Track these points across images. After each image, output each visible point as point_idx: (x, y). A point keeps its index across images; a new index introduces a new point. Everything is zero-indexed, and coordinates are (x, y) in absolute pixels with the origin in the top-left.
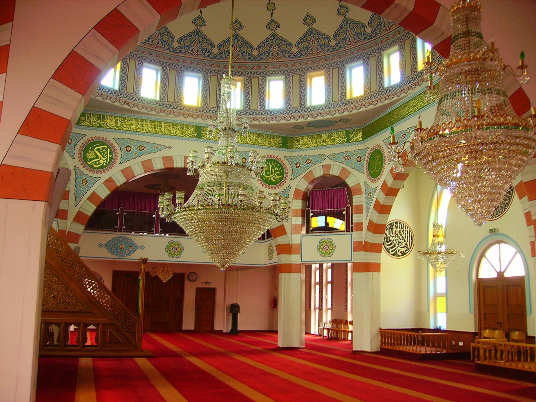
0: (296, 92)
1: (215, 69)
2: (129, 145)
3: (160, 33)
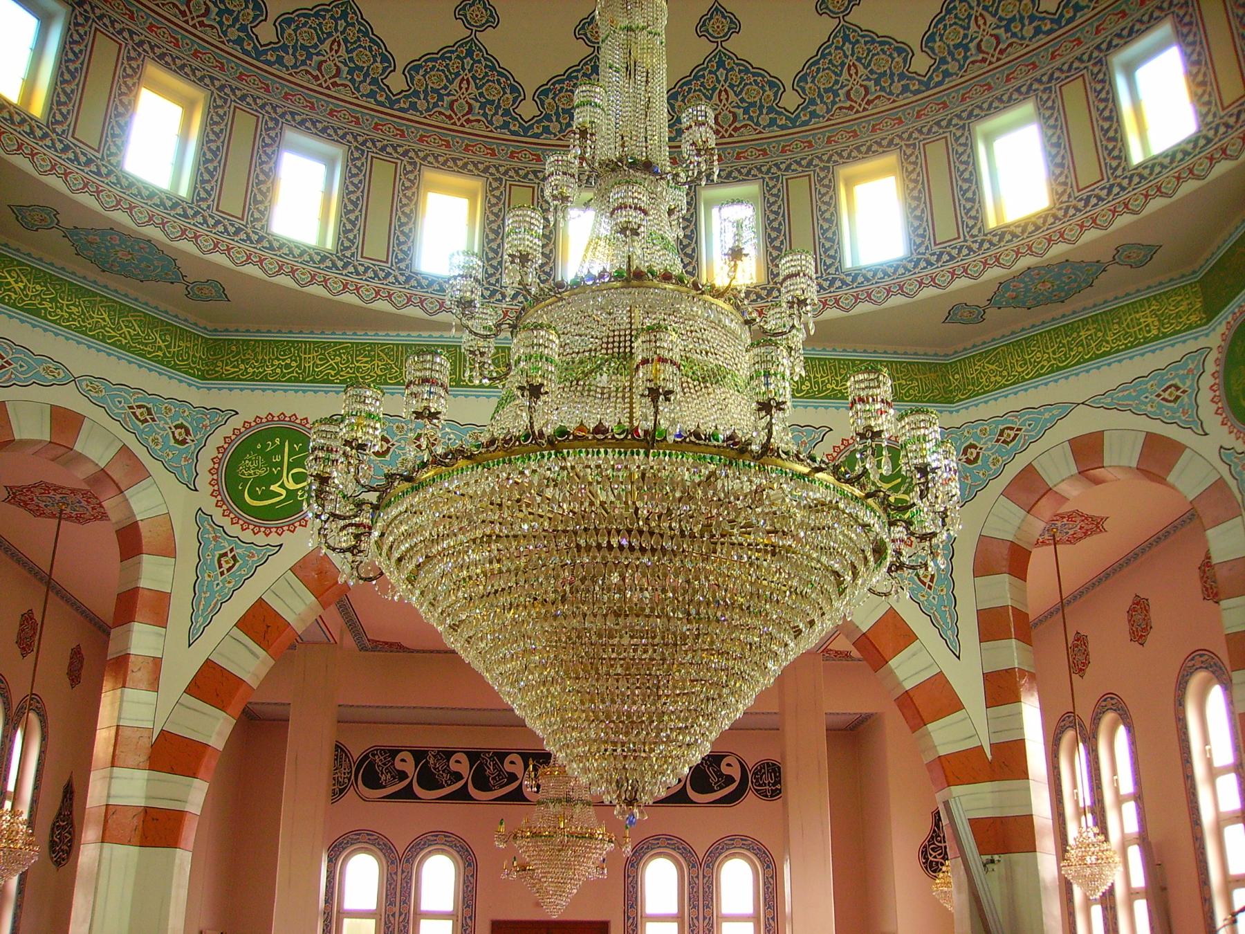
0: (946, 189)
1: (476, 159)
2: (971, 441)
3: (474, 77)
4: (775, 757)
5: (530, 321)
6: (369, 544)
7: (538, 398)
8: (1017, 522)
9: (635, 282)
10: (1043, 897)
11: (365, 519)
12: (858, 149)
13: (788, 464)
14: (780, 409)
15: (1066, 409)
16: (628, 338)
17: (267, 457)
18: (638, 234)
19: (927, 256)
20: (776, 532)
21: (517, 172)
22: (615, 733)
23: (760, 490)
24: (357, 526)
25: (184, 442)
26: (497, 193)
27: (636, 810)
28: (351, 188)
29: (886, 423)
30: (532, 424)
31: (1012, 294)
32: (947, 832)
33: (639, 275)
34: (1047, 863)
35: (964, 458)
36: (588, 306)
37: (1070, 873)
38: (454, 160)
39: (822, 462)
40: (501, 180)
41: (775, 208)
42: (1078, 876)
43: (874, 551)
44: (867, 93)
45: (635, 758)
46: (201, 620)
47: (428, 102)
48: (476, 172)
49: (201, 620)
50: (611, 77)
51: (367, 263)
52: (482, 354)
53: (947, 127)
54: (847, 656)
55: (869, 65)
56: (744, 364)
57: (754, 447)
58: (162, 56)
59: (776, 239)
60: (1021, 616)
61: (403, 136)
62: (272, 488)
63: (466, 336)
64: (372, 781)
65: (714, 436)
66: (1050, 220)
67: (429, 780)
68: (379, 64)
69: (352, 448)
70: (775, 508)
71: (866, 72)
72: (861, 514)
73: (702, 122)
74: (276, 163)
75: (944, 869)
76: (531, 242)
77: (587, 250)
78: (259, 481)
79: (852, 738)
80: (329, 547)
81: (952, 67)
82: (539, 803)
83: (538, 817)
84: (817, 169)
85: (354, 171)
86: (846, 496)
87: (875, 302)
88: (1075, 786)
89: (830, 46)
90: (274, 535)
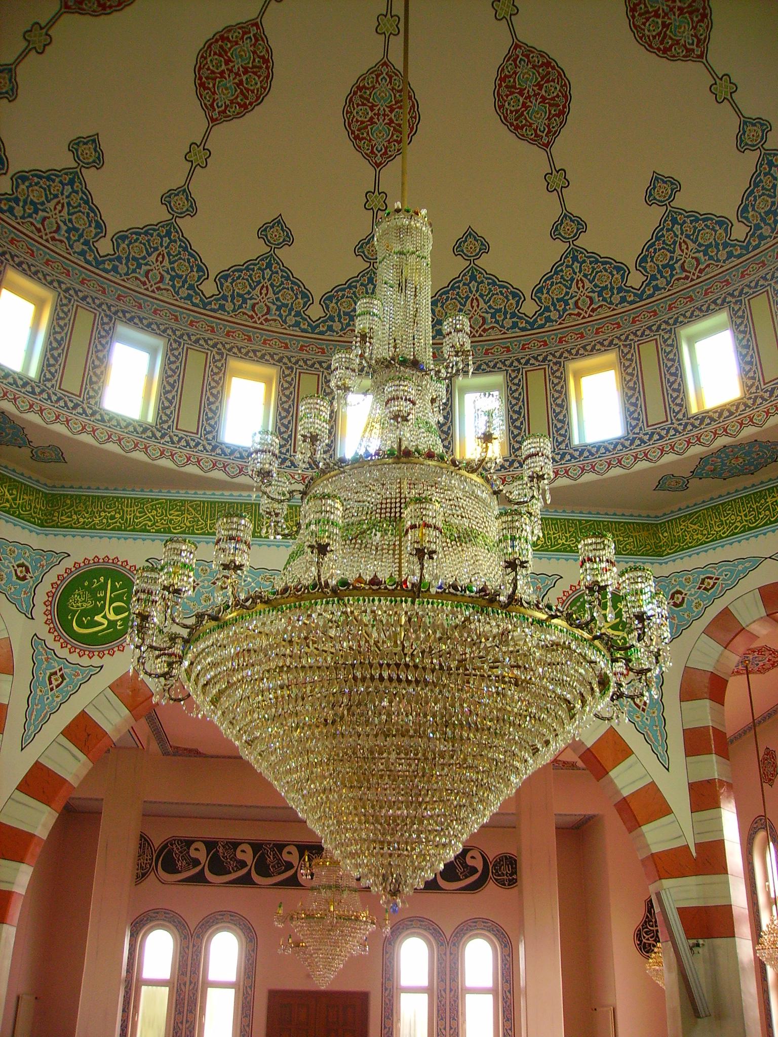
0: (655, 383)
1: (272, 351)
2: (678, 588)
4: (511, 850)
5: (318, 490)
6: (180, 671)
7: (325, 555)
8: (716, 656)
9: (403, 459)
10: (741, 977)
11: (178, 649)
12: (584, 347)
13: (529, 612)
14: (524, 567)
15: (756, 562)
16: (398, 505)
17: (93, 593)
18: (407, 421)
19: (641, 435)
20: (518, 667)
21: (305, 362)
22: (383, 834)
23: (505, 633)
24: (170, 655)
25: (24, 578)
26: (289, 379)
27: (399, 900)
28: (170, 373)
29: (610, 579)
30: (319, 576)
31: (713, 467)
32: (659, 918)
33: (407, 453)
34: (745, 948)
35: (672, 602)
36: (365, 478)
37: (764, 956)
38: (254, 351)
39: (557, 610)
40: (292, 368)
41: (516, 395)
42: (770, 959)
43: (600, 683)
44: (592, 302)
45: (399, 856)
46: (32, 728)
47: (234, 304)
48: (272, 362)
49: (32, 728)
50: (387, 292)
51: (181, 434)
52: (277, 515)
53: (657, 330)
54: (573, 765)
55: (593, 280)
56: (493, 529)
57: (502, 598)
58: (20, 264)
59: (518, 422)
60: (720, 735)
61: (213, 331)
62: (96, 618)
63: (264, 500)
64: (170, 867)
65: (468, 588)
66: (742, 407)
67: (218, 867)
68: (195, 273)
69: (169, 593)
70: (517, 648)
71: (591, 286)
72: (589, 653)
73: (460, 329)
74: (109, 351)
75: (656, 950)
76: (321, 426)
77: (365, 431)
78: (85, 613)
79: (577, 835)
80: (146, 673)
81: (661, 282)
82: (313, 889)
83: (313, 902)
84: (551, 364)
85: (173, 359)
86: (576, 639)
87: (598, 473)
88: (766, 879)
89: (562, 265)
90: (96, 658)
